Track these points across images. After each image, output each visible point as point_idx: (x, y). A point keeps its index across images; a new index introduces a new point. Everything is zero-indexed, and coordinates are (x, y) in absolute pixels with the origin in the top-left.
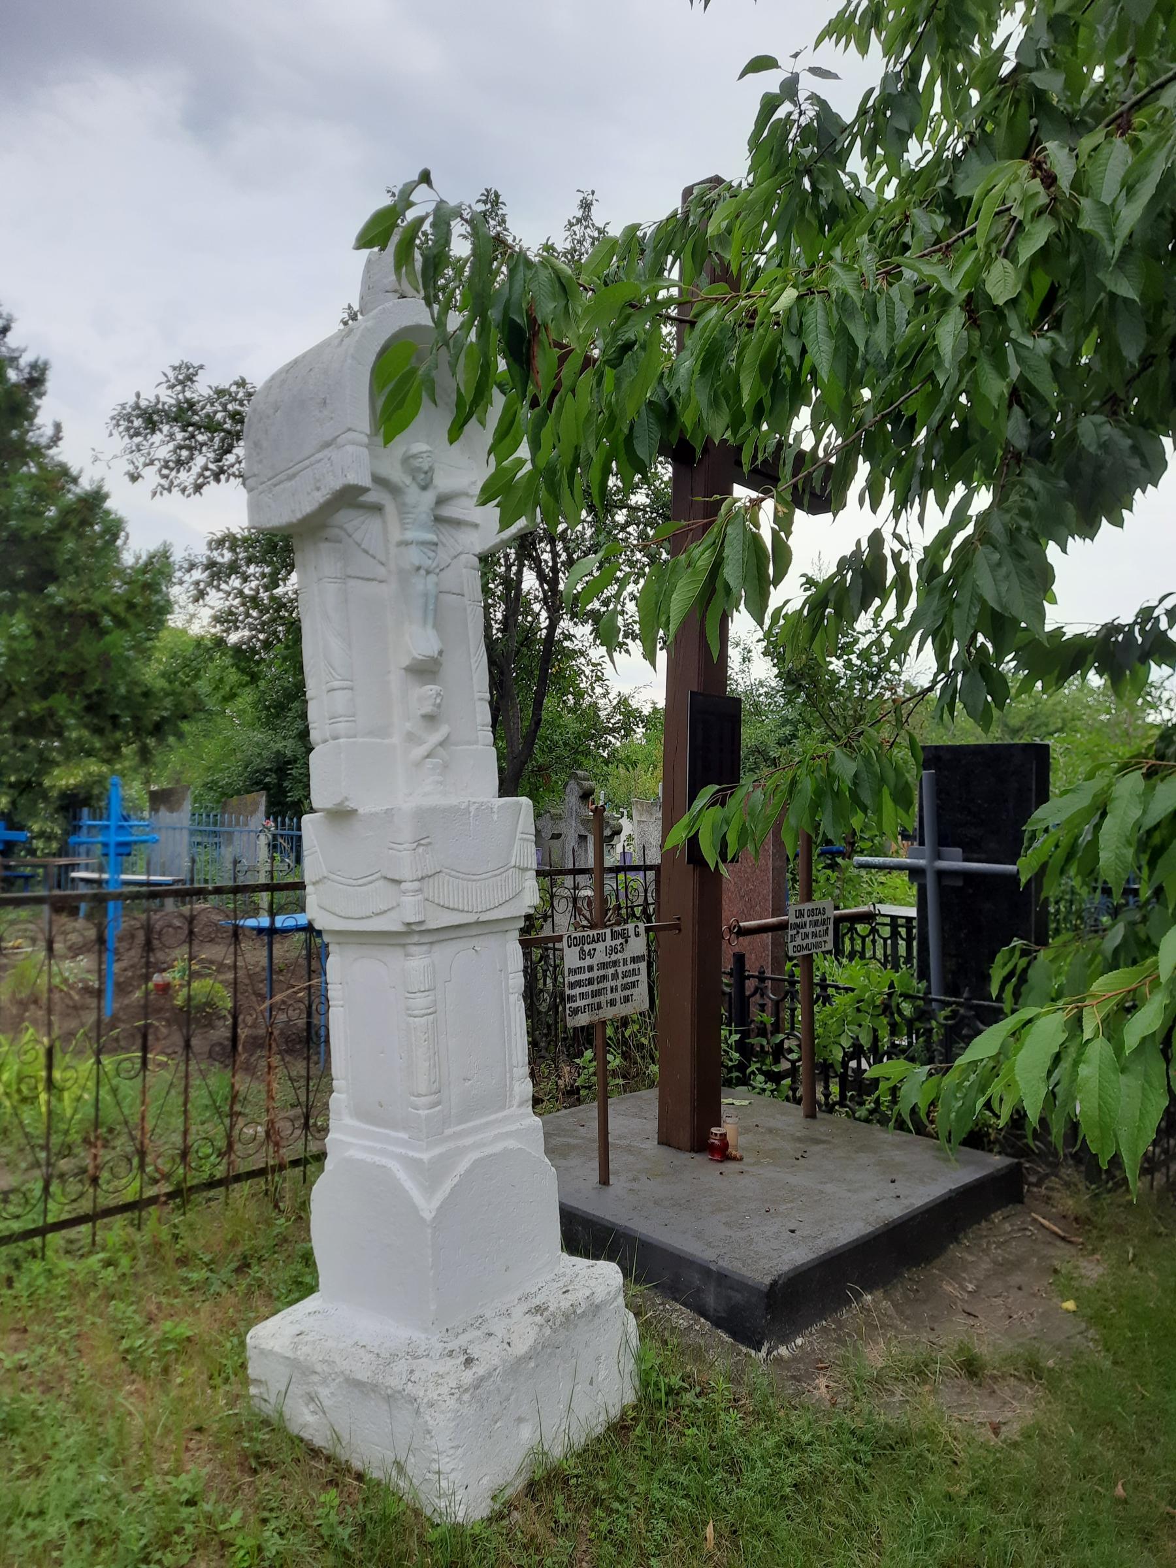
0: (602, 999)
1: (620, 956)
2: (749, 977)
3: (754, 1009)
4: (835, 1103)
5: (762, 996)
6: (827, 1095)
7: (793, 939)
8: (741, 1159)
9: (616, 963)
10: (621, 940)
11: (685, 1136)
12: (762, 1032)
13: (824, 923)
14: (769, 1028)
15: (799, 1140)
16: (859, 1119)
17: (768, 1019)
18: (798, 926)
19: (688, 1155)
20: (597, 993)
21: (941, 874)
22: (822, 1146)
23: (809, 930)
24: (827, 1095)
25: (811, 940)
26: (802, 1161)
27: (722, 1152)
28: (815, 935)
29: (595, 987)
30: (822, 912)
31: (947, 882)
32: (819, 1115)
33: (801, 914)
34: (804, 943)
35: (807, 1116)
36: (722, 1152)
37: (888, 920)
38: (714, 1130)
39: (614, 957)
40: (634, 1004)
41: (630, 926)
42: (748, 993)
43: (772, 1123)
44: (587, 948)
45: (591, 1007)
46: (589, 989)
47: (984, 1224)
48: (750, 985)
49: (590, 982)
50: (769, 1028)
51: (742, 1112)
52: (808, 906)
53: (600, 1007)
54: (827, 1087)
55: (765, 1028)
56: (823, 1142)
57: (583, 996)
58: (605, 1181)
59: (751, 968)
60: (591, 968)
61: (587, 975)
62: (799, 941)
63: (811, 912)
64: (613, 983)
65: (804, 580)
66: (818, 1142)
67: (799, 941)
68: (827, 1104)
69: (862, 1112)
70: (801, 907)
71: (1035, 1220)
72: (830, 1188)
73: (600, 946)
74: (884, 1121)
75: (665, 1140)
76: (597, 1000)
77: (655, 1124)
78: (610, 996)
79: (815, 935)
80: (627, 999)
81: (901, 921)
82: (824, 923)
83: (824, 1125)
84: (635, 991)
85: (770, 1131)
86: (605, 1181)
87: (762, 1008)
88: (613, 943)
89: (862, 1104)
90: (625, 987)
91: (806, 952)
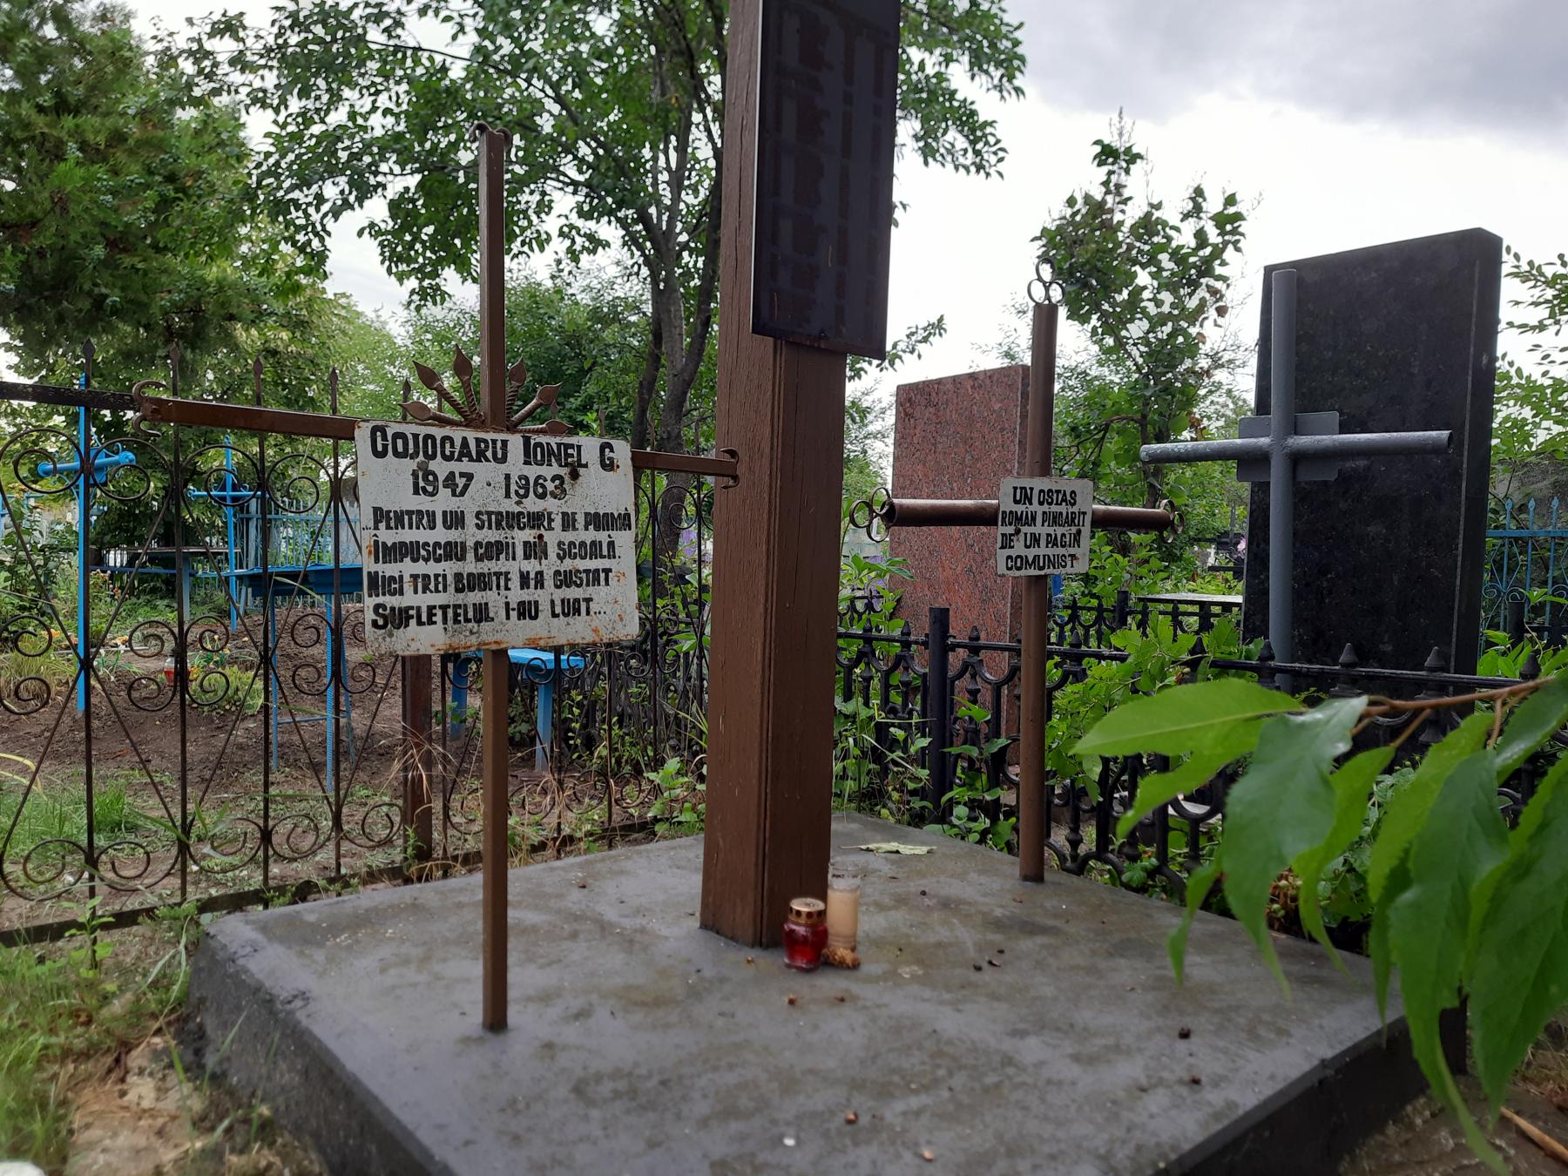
0: (493, 598)
1: (550, 504)
2: (953, 647)
3: (961, 697)
4: (1088, 857)
5: (973, 676)
6: (1075, 843)
7: (1007, 542)
8: (855, 966)
9: (536, 520)
10: (555, 469)
11: (743, 915)
12: (973, 737)
13: (1071, 520)
14: (985, 729)
15: (998, 925)
16: (1127, 886)
17: (982, 714)
18: (1017, 519)
19: (752, 954)
20: (478, 582)
21: (1298, 459)
22: (1040, 940)
23: (1040, 529)
24: (1075, 843)
25: (1042, 550)
26: (988, 975)
27: (814, 951)
28: (1052, 541)
29: (470, 566)
30: (1071, 499)
31: (1307, 475)
32: (1047, 876)
33: (1024, 496)
34: (1030, 553)
35: (1026, 878)
36: (814, 951)
37: (1196, 609)
38: (799, 905)
39: (532, 504)
40: (596, 621)
41: (589, 445)
42: (950, 674)
43: (953, 888)
44: (440, 467)
45: (455, 615)
46: (449, 568)
47: (1391, 1129)
48: (956, 659)
49: (453, 551)
50: (985, 729)
51: (877, 873)
52: (1040, 484)
53: (482, 613)
54: (1075, 829)
55: (977, 732)
56: (1044, 930)
57: (423, 583)
58: (496, 1020)
59: (958, 631)
60: (455, 520)
61: (441, 535)
62: (1019, 548)
63: (1047, 497)
64: (531, 566)
65: (1098, 149)
66: (1030, 928)
67: (1019, 548)
68: (1075, 857)
69: (1134, 873)
70: (1026, 482)
71: (1504, 1119)
72: (1031, 1049)
73: (485, 471)
74: (1175, 891)
75: (713, 920)
76: (474, 597)
77: (697, 880)
78: (516, 595)
79: (1052, 541)
80: (572, 608)
81: (1216, 610)
82: (1071, 520)
83: (1058, 897)
84: (599, 593)
85: (946, 904)
86: (496, 1020)
87: (974, 695)
88: (533, 471)
89: (1134, 858)
90: (565, 579)
91: (1033, 572)
